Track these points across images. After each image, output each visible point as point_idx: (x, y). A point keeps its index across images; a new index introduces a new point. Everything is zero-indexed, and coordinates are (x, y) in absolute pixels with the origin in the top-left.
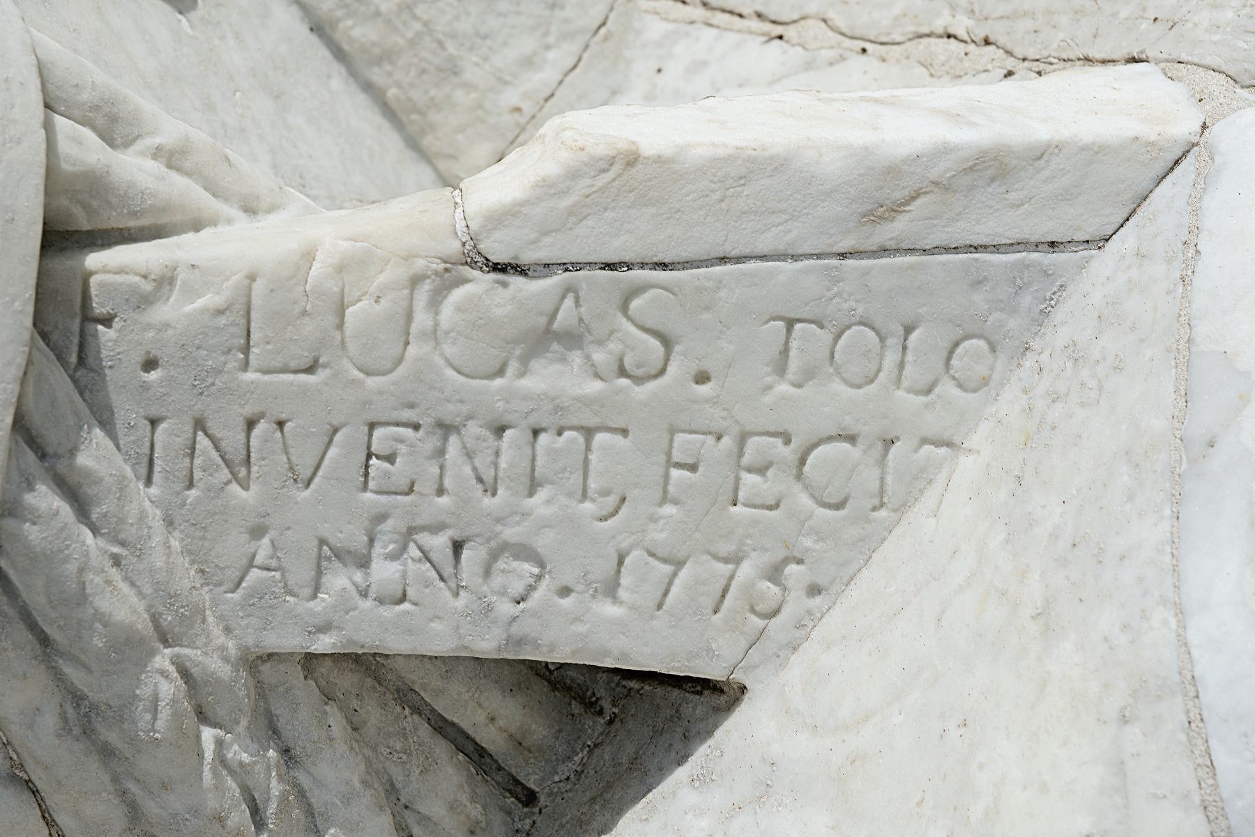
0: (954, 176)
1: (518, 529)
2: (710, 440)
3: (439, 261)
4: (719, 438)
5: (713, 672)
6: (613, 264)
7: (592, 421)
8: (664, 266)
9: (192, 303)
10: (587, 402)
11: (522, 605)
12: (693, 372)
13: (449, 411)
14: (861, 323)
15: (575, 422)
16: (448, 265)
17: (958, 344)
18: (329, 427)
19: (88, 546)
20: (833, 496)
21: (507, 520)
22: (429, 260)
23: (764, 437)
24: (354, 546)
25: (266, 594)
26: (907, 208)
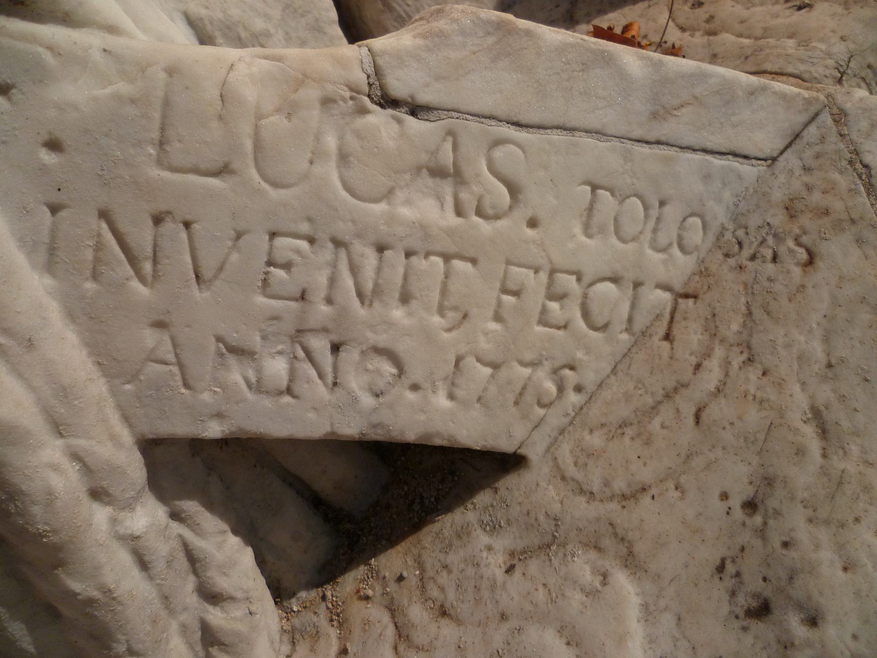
0: (708, 95)
1: (385, 336)
2: (531, 273)
3: (345, 88)
4: (536, 271)
5: (506, 446)
6: (479, 115)
7: (453, 249)
8: (517, 124)
9: (103, 89)
10: (450, 232)
11: (381, 400)
12: (527, 218)
13: (343, 229)
14: (636, 195)
15: (438, 248)
16: (354, 94)
17: (55, 470)
18: (233, 232)
19: (206, 563)
20: (600, 321)
21: (378, 327)
22: (338, 86)
23: (565, 274)
24: (247, 345)
25: (162, 387)
26: (675, 112)
